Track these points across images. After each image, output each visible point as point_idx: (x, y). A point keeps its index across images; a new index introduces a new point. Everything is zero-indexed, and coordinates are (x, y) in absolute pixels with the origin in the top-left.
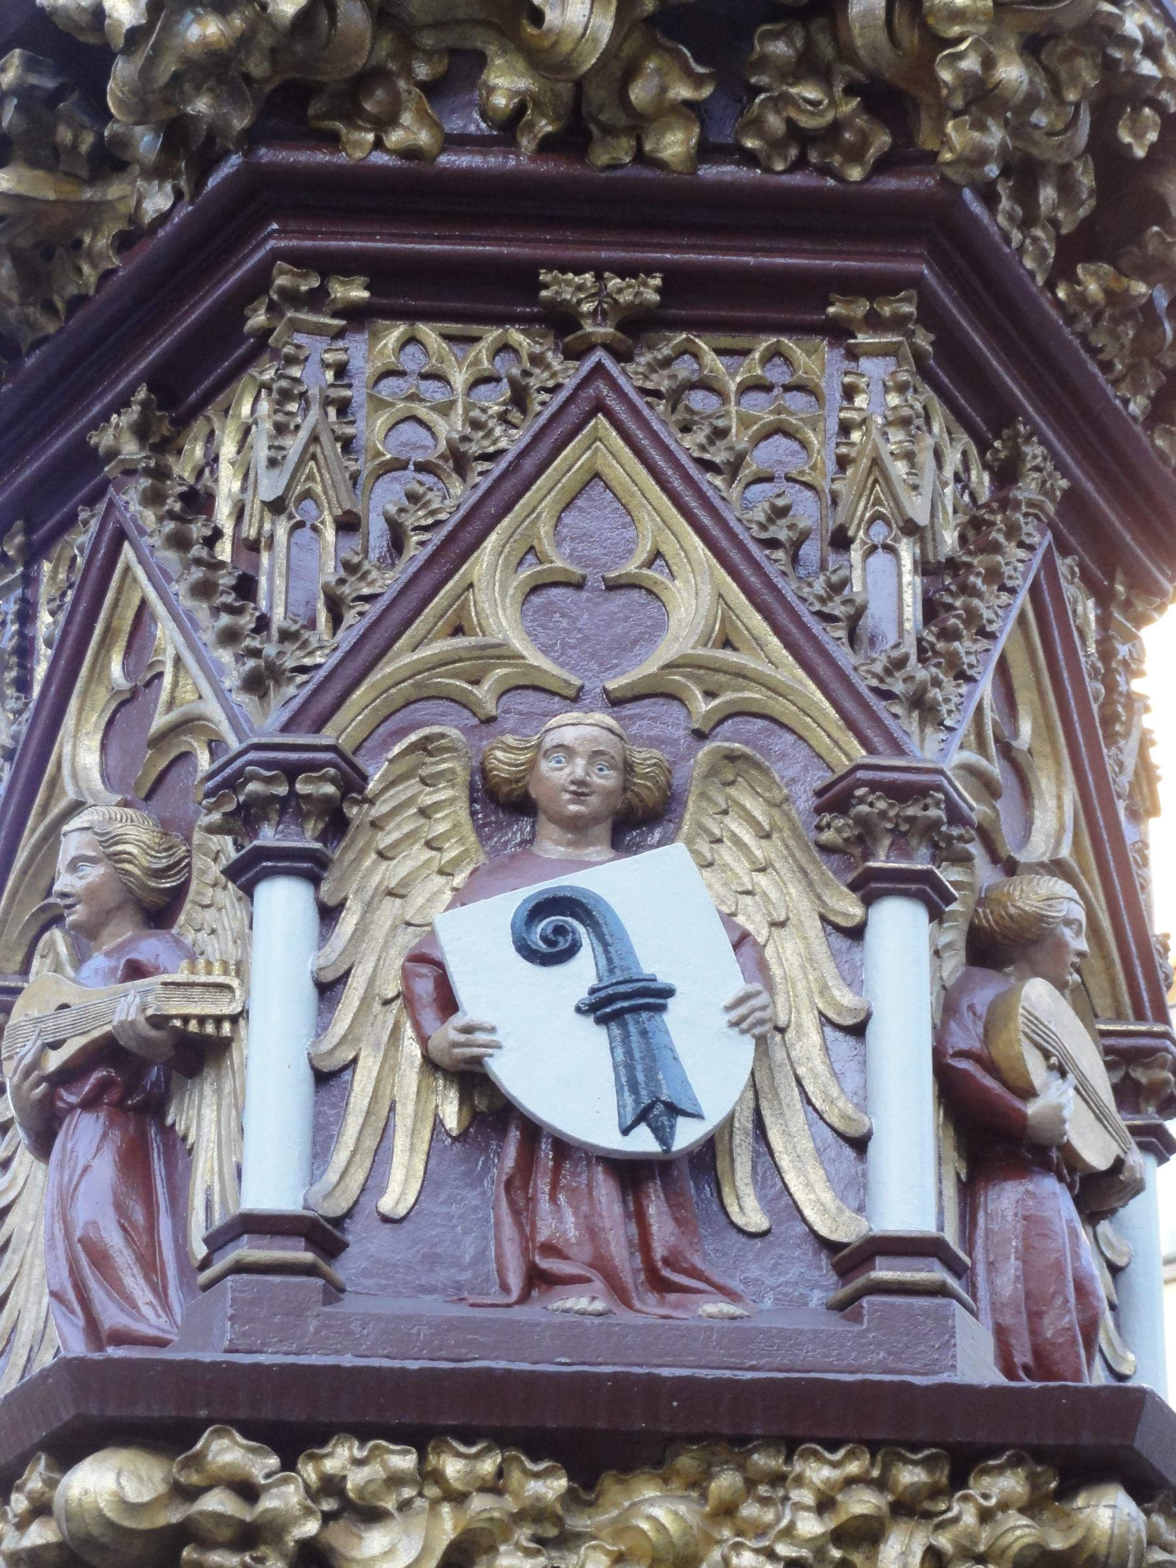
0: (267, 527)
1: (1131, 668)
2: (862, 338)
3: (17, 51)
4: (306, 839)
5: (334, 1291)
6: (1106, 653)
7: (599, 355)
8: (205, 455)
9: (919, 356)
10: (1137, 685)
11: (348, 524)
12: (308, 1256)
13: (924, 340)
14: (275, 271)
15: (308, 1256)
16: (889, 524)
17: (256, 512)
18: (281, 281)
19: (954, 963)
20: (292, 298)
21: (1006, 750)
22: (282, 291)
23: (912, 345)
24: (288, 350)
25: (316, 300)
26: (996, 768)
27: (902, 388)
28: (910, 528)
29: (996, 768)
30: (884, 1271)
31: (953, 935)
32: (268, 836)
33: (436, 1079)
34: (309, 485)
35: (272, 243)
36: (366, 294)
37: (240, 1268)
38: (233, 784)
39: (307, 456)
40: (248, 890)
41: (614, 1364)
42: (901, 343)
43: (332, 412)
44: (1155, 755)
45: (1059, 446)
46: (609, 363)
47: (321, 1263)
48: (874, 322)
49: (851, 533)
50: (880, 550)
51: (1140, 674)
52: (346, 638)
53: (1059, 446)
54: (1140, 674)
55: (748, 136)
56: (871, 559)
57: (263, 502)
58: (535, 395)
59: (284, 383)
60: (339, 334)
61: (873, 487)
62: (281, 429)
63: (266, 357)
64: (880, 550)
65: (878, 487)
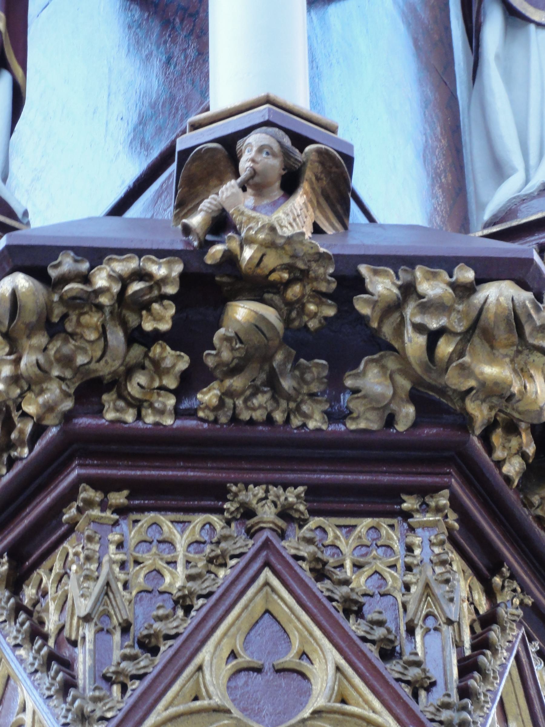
0: (81, 632)
3: (181, 408)
7: (266, 534)
9: (450, 529)
13: (452, 519)
14: (81, 488)
18: (82, 495)
20: (89, 504)
22: (85, 501)
23: (446, 523)
28: (449, 622)
33: (259, 342)
34: (105, 607)
35: (76, 472)
42: (439, 520)
46: (275, 540)
48: (425, 508)
49: (416, 622)
50: (432, 631)
52: (130, 699)
55: (59, 432)
56: (427, 637)
57: (79, 618)
58: (281, 211)
60: (116, 523)
61: (426, 598)
64: (432, 631)
65: (429, 598)
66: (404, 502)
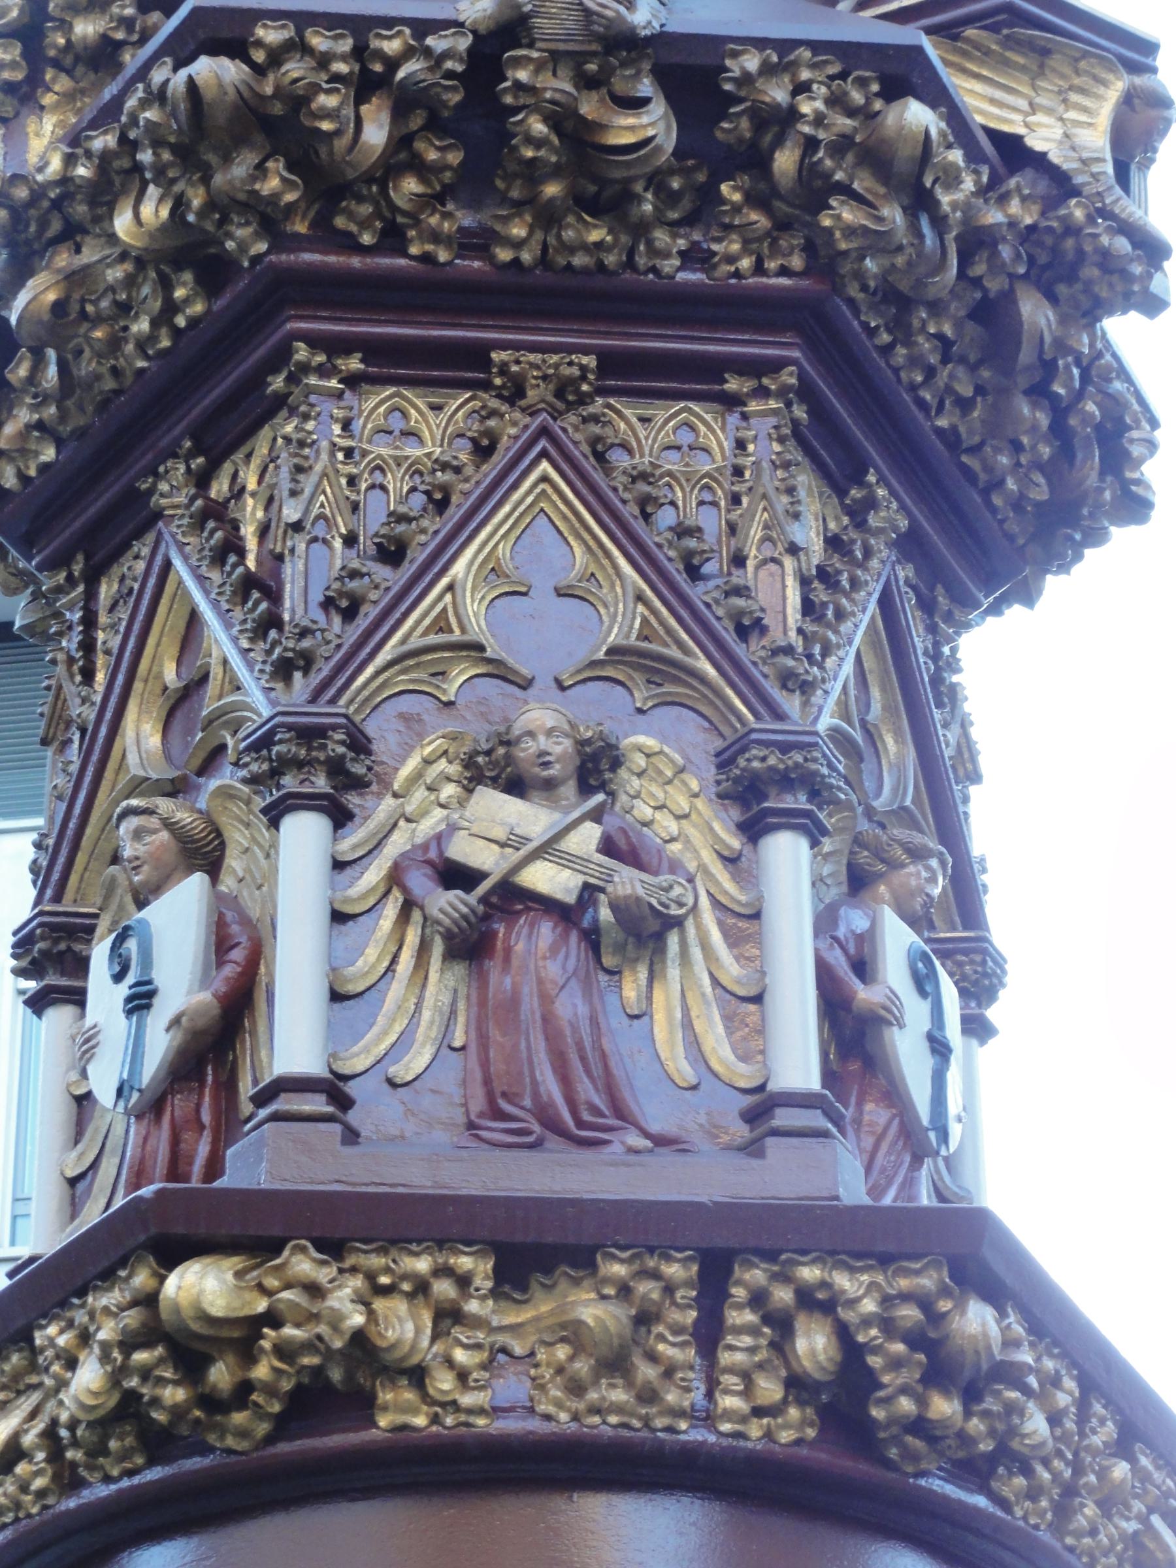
1: (953, 665)
2: (753, 406)
4: (321, 783)
5: (351, 1136)
6: (936, 656)
8: (231, 489)
9: (795, 423)
10: (955, 679)
11: (350, 540)
12: (330, 1109)
15: (330, 1109)
16: (775, 544)
17: (281, 531)
19: (834, 893)
20: (305, 368)
21: (864, 723)
24: (303, 408)
25: (323, 372)
26: (858, 736)
27: (781, 440)
29: (858, 736)
30: (783, 1118)
31: (835, 869)
32: (290, 782)
36: (362, 366)
37: (276, 1117)
38: (264, 743)
39: (318, 489)
40: (274, 823)
41: (784, 587)
43: (340, 456)
44: (975, 733)
45: (908, 501)
47: (339, 1114)
48: (762, 392)
51: (958, 671)
53: (908, 501)
54: (958, 671)
59: (301, 435)
62: (299, 469)
63: (284, 413)
66: (726, 381)
